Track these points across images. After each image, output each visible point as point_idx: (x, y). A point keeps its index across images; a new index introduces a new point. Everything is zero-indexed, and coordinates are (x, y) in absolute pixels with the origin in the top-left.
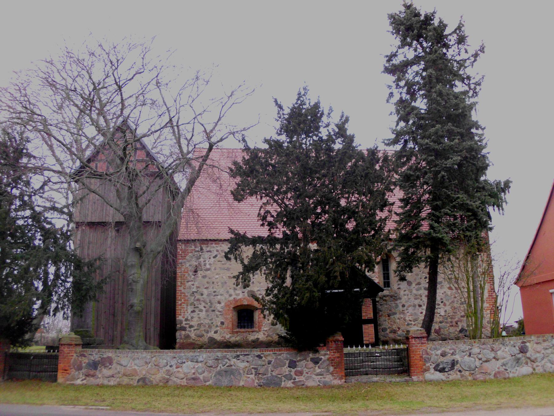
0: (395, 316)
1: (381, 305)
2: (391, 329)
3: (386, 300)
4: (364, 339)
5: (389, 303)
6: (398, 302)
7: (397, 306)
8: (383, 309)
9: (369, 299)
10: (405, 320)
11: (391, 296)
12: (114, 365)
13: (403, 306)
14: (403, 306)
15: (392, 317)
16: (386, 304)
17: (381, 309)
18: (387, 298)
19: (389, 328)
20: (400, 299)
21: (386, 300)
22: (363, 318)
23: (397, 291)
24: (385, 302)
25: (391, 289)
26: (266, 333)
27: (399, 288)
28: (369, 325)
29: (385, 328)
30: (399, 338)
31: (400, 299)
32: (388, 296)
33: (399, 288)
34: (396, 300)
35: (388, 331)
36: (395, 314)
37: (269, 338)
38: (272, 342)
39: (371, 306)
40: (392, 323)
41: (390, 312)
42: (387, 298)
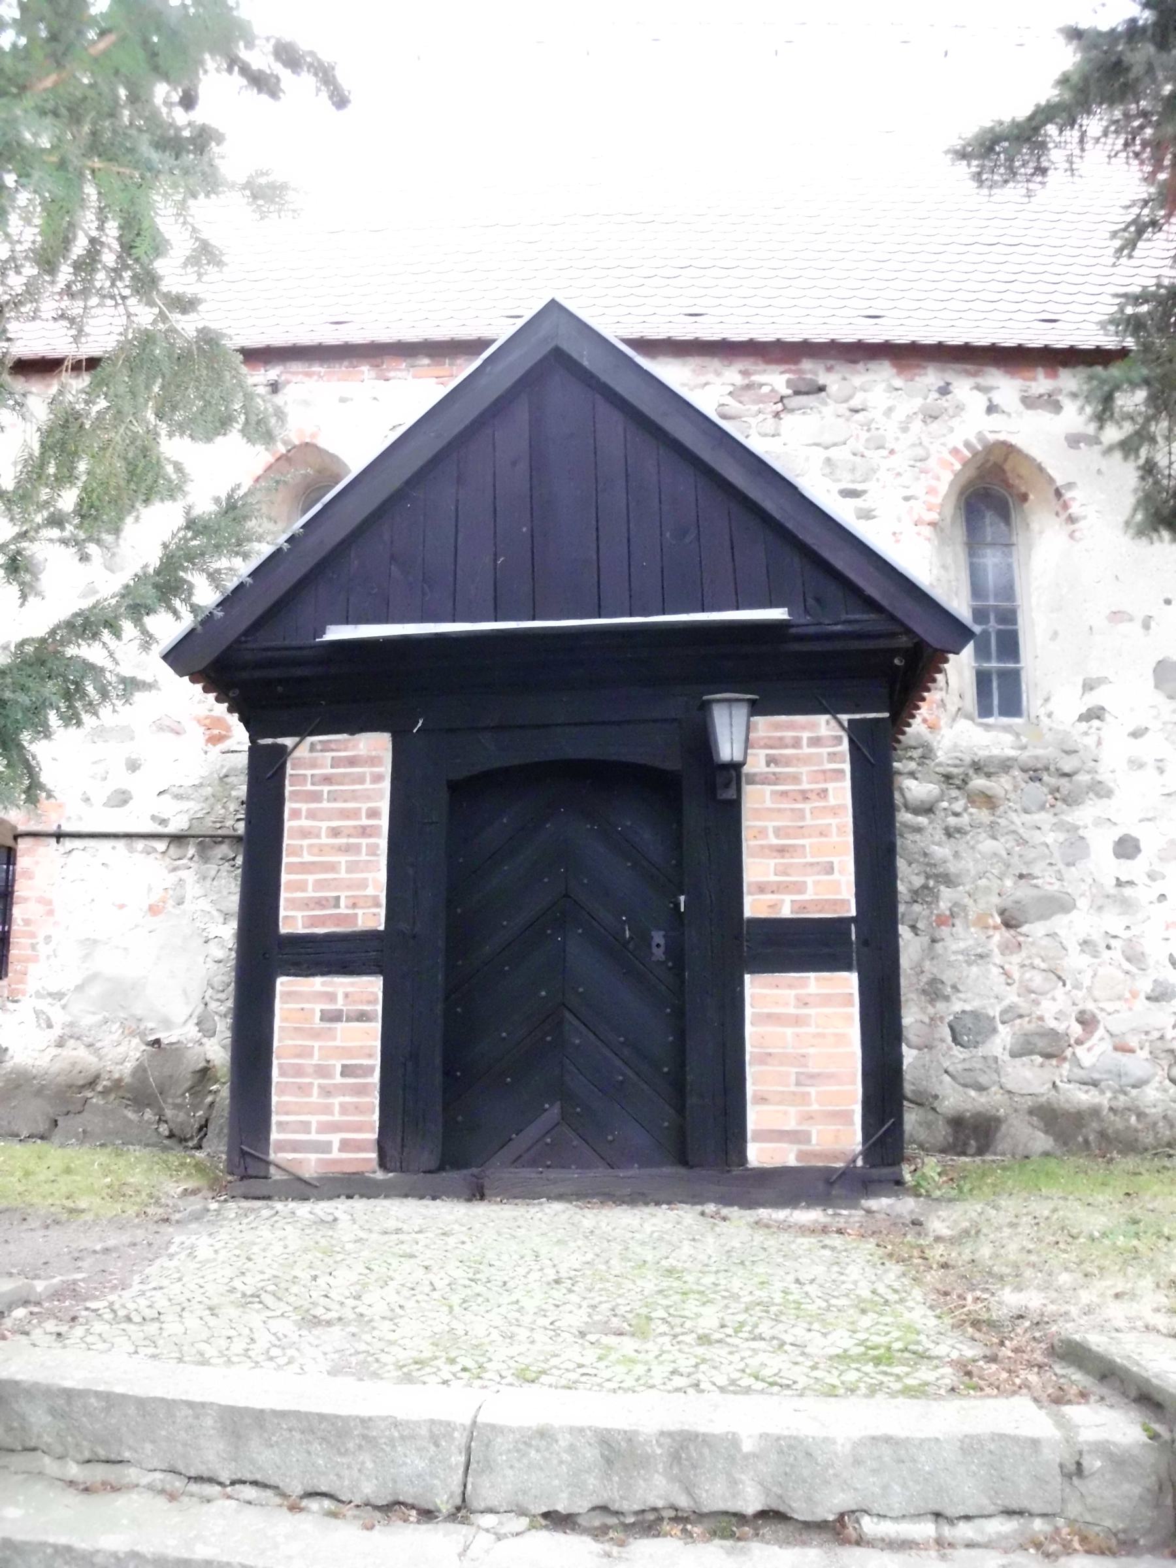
0: (1059, 923)
1: (949, 833)
2: (1024, 1025)
3: (988, 801)
4: (755, 1117)
5: (1018, 819)
6: (1084, 814)
7: (1076, 846)
8: (967, 865)
9: (824, 725)
10: (1135, 957)
11: (1034, 773)
12: (1081, 1007)
13: (1127, 848)
14: (1127, 848)
15: (1035, 930)
16: (993, 831)
17: (952, 867)
18: (1000, 785)
19: (1011, 1014)
20: (1100, 790)
21: (988, 801)
22: (754, 907)
23: (1083, 737)
24: (984, 815)
25: (1036, 723)
26: (59, 1017)
27: (1095, 714)
28: (814, 982)
29: (976, 1015)
30: (1084, 1098)
31: (1100, 790)
32: (1006, 765)
33: (1095, 714)
34: (1071, 800)
35: (1002, 1040)
36: (1061, 905)
37: (78, 1054)
38: (92, 1083)
39: (842, 793)
40: (1037, 980)
41: (1023, 892)
42: (1000, 785)
